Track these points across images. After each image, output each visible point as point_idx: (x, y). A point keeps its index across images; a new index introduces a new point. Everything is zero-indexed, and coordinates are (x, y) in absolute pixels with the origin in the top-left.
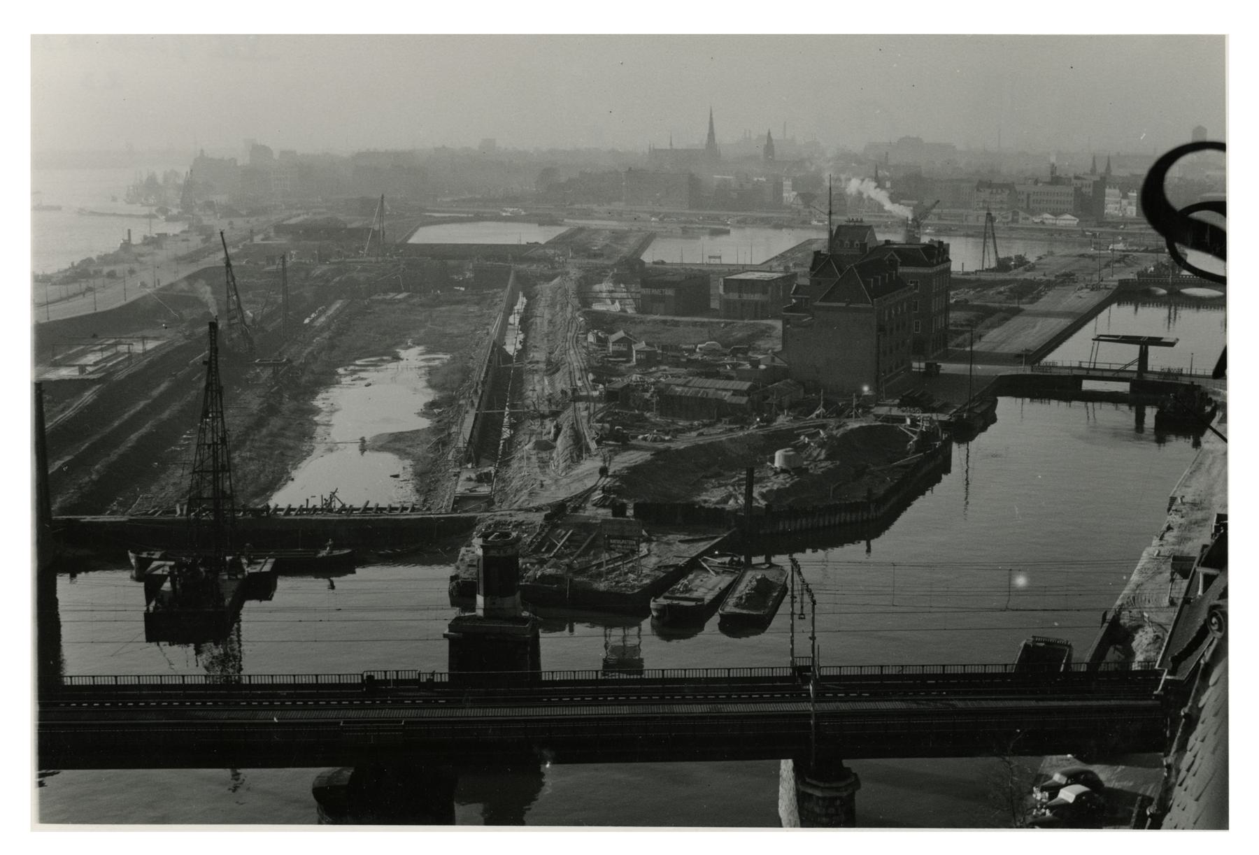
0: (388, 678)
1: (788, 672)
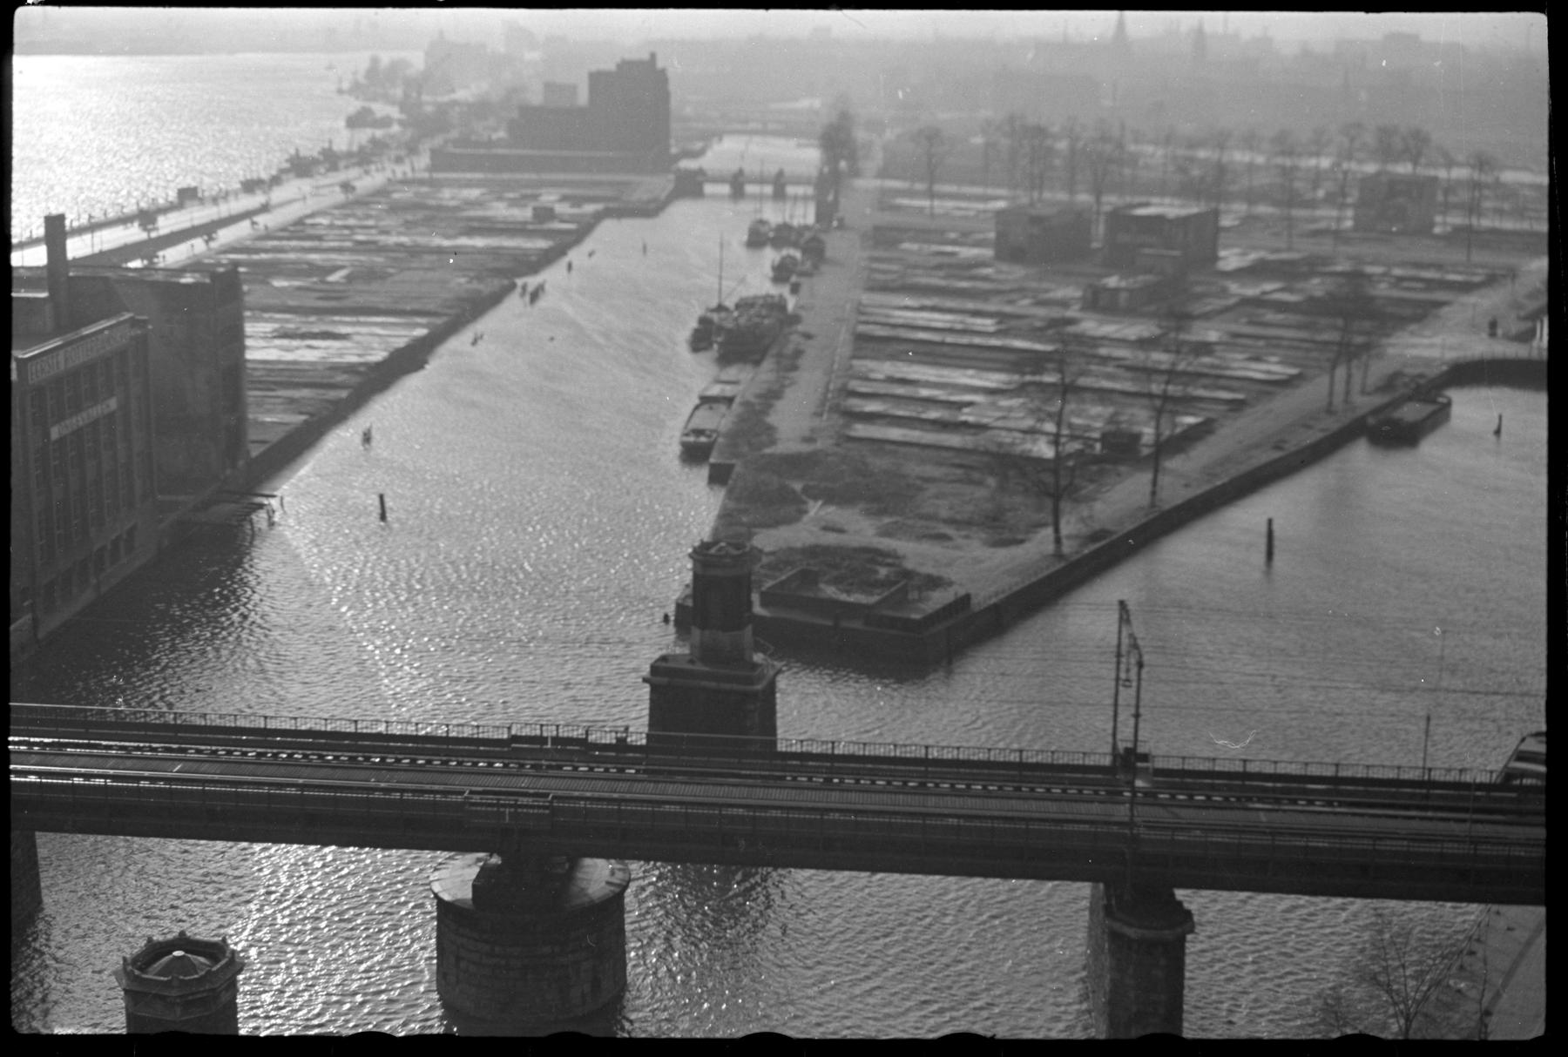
0: (545, 734)
1: (1107, 761)
